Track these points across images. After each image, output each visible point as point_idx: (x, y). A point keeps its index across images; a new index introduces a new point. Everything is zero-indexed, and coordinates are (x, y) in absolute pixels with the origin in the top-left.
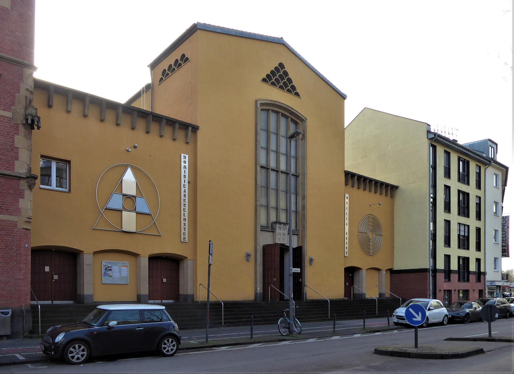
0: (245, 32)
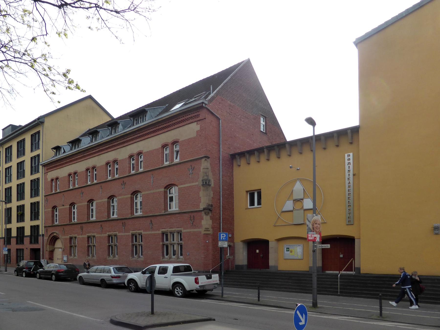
0: (378, 26)
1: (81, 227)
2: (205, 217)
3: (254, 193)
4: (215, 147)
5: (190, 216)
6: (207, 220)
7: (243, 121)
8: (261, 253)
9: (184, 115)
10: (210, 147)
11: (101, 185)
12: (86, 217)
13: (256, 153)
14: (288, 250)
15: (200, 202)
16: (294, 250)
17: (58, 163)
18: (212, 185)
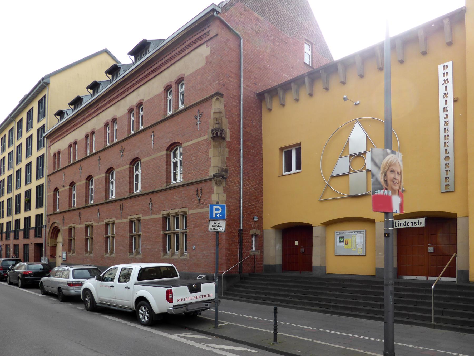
1: (79, 213)
2: (215, 188)
3: (291, 151)
4: (232, 80)
5: (197, 188)
6: (218, 194)
7: (278, 46)
8: (302, 247)
9: (190, 37)
10: (225, 80)
11: (99, 156)
12: (84, 200)
13: (293, 86)
14: (341, 240)
15: (210, 166)
16: (351, 242)
17: (59, 132)
18: (228, 139)
